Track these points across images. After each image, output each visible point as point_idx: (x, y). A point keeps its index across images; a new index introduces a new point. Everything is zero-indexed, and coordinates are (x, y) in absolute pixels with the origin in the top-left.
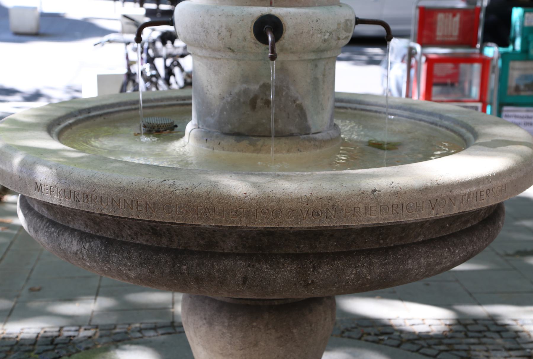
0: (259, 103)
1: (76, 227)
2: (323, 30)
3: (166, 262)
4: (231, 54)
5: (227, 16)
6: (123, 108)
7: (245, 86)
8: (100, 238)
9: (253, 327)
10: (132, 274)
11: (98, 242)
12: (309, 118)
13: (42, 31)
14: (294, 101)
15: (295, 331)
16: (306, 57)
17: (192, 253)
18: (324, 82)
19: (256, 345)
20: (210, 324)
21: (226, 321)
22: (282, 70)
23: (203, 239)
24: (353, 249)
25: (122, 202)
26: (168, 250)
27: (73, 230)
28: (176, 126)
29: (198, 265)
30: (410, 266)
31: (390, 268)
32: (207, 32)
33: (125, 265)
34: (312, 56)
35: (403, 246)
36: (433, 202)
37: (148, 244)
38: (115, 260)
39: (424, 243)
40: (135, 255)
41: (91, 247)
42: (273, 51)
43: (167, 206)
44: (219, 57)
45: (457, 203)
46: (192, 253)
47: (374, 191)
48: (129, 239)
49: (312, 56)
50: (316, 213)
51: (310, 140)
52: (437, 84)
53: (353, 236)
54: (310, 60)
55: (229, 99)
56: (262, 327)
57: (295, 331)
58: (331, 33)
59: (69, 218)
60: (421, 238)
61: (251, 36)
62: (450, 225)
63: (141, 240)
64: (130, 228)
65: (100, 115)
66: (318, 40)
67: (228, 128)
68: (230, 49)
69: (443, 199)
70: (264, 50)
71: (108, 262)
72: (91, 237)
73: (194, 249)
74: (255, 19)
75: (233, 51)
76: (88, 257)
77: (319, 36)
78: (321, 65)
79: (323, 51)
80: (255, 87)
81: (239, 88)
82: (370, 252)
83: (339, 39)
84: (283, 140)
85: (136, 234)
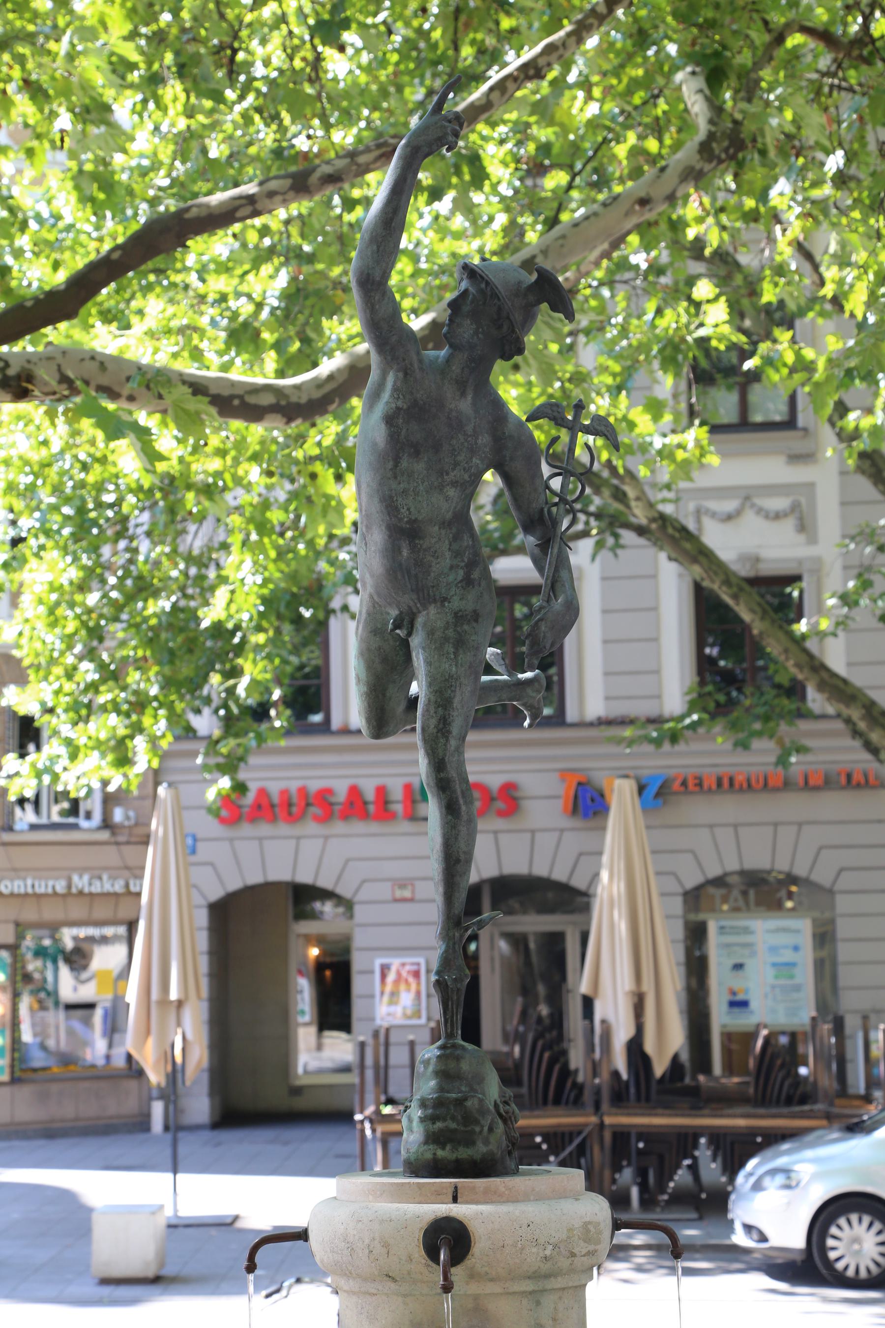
2: (541, 1241)
4: (393, 1285)
5: (382, 1222)
13: (167, 1271)
16: (517, 1287)
34: (529, 1286)
42: (446, 1278)
44: (373, 1291)
49: (529, 1286)
54: (523, 1292)
58: (555, 1246)
61: (419, 1253)
66: (532, 1258)
68: (388, 1276)
75: (394, 1280)
77: (534, 1250)
78: (548, 1302)
83: (573, 1255)
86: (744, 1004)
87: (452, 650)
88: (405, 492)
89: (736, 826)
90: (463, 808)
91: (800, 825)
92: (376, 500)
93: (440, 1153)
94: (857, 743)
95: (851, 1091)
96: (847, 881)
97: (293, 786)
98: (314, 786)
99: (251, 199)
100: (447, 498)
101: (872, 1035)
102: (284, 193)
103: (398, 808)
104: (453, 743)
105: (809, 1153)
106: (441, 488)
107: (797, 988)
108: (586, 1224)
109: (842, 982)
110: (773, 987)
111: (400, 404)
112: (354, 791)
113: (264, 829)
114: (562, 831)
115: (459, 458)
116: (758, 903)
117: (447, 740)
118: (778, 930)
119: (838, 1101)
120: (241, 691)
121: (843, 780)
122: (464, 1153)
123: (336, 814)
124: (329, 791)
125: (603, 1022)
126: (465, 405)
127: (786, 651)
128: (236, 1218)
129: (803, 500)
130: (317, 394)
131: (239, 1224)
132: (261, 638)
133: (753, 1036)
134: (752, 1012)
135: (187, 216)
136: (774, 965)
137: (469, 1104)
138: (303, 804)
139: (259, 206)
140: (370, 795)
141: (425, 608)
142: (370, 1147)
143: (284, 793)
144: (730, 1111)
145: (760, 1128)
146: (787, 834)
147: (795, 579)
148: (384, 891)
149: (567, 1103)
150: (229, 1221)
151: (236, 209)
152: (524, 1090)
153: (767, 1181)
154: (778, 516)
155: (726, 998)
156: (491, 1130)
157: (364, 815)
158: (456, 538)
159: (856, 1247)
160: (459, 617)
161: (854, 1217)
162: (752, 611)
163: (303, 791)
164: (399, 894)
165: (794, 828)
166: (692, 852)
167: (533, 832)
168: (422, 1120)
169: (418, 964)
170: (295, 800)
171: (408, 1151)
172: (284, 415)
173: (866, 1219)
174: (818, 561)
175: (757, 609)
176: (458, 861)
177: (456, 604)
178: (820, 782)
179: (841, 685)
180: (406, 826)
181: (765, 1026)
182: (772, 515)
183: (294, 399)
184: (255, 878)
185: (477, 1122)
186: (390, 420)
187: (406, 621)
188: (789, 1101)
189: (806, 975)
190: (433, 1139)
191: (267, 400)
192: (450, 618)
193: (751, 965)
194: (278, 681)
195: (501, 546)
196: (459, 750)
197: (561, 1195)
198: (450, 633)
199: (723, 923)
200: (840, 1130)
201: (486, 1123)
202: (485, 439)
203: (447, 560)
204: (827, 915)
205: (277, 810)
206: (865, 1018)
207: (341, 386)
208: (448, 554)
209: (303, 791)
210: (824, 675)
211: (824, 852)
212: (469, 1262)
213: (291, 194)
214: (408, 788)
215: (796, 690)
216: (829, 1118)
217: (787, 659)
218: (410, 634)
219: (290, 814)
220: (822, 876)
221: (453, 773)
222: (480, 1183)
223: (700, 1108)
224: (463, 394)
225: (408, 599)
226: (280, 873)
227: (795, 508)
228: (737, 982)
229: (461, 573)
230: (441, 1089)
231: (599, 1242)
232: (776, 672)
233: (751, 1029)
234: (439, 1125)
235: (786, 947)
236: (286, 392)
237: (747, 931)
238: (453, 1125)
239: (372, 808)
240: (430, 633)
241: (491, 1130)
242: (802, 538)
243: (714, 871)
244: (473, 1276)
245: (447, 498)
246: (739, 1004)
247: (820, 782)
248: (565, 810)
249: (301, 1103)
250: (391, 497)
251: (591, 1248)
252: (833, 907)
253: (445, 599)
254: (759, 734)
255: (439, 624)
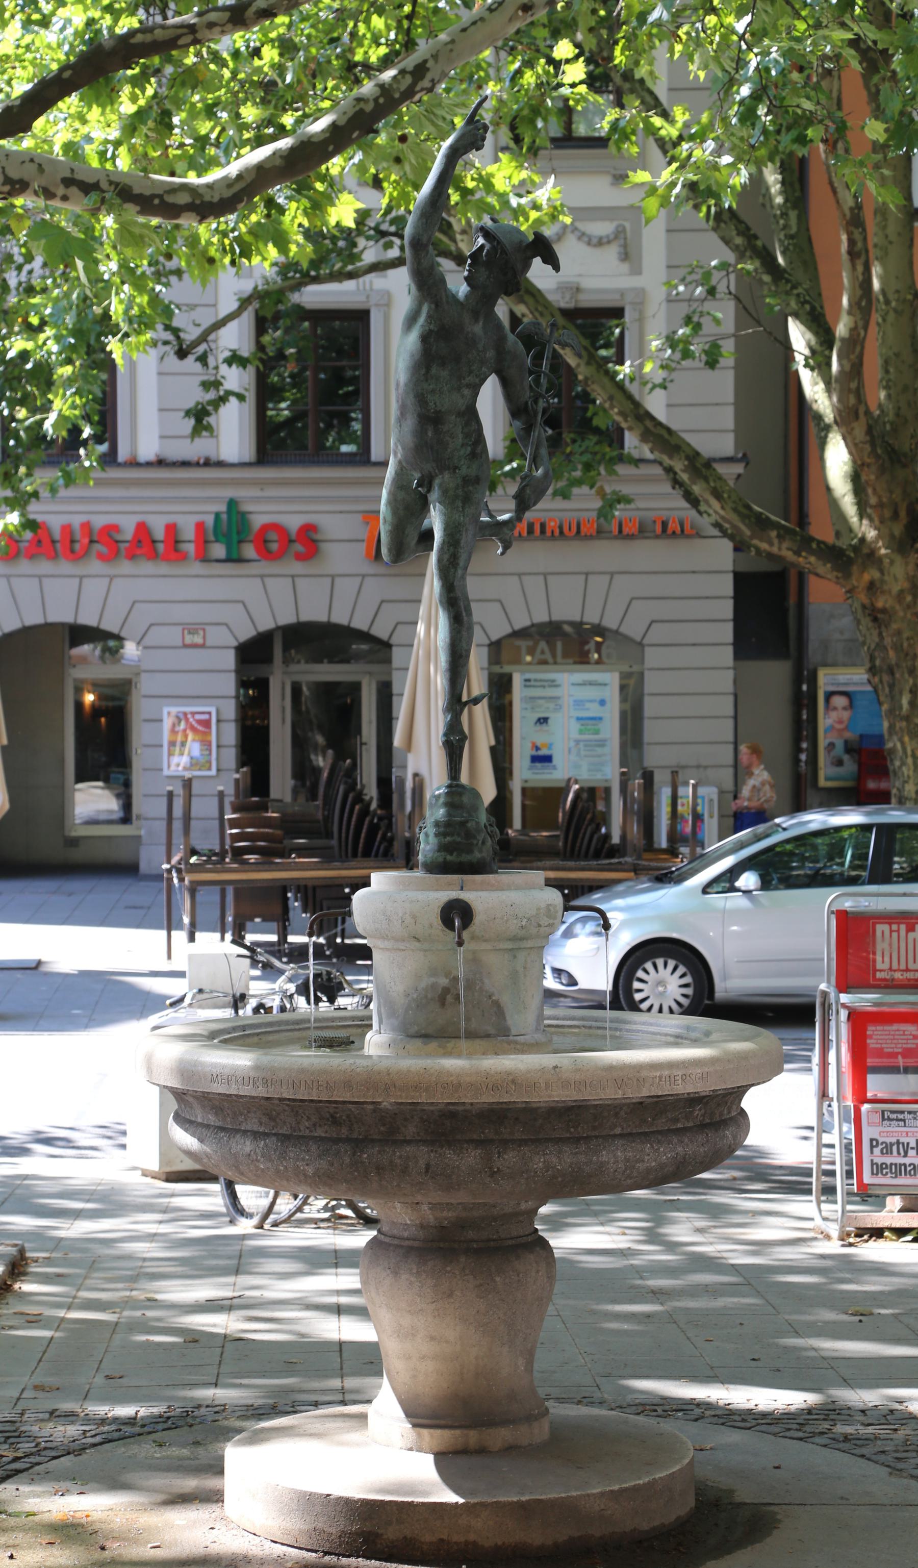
0: (449, 999)
1: (249, 1128)
3: (346, 1151)
4: (417, 944)
5: (412, 902)
6: (283, 1028)
7: (433, 980)
8: (275, 1134)
9: (447, 1272)
10: (310, 1171)
11: (274, 1138)
12: (508, 1018)
14: (490, 997)
15: (498, 1279)
17: (373, 1141)
18: (525, 976)
19: (450, 1295)
20: (396, 1273)
21: (414, 1267)
22: (474, 960)
23: (384, 1125)
24: (541, 1136)
25: (303, 1083)
26: (348, 1140)
27: (245, 1132)
28: (353, 1042)
29: (379, 1152)
30: (605, 1159)
31: (582, 1158)
32: (389, 920)
33: (303, 1159)
34: (509, 945)
35: (596, 1137)
36: (619, 1082)
37: (327, 1135)
38: (292, 1155)
39: (621, 1136)
40: (313, 1147)
41: (266, 1145)
42: (460, 937)
43: (348, 1084)
45: (647, 1085)
46: (373, 1141)
47: (556, 1067)
48: (307, 1133)
49: (509, 945)
50: (495, 1087)
51: (509, 1043)
52: (877, 1070)
53: (540, 1121)
55: (415, 996)
56: (457, 1272)
57: (498, 1279)
58: (529, 919)
59: (241, 1119)
60: (618, 1131)
61: (437, 922)
62: (653, 1120)
63: (320, 1132)
64: (309, 1119)
65: (258, 1034)
67: (414, 1029)
69: (629, 1079)
70: (452, 936)
71: (285, 1158)
72: (266, 1135)
73: (375, 1137)
74: (442, 904)
75: (418, 940)
76: (263, 1156)
78: (521, 956)
79: (522, 939)
80: (444, 982)
81: (426, 982)
82: (560, 1140)
83: (540, 926)
84: (478, 1042)
85: (314, 1125)
86: (548, 759)
87: (460, 504)
88: (433, 391)
89: (545, 575)
90: (465, 618)
91: (612, 574)
92: (411, 396)
93: (449, 858)
94: (678, 493)
95: (656, 846)
96: (657, 634)
97: (76, 521)
98: (99, 522)
99: (191, 29)
100: (463, 396)
101: (681, 791)
102: (224, 25)
103: (190, 548)
104: (460, 572)
105: (619, 902)
106: (459, 389)
107: (602, 743)
108: (549, 905)
109: (647, 737)
110: (577, 742)
111: (432, 327)
112: (142, 529)
113: (44, 566)
114: (364, 576)
115: (473, 368)
116: (565, 655)
117: (456, 570)
118: (584, 684)
119: (647, 855)
120: (48, 426)
121: (658, 528)
122: (465, 858)
123: (123, 552)
124: (115, 528)
125: (416, 775)
126: (478, 329)
127: (611, 398)
128: (39, 963)
129: (627, 225)
130: (228, 194)
131: (43, 969)
132: (67, 370)
133: (565, 790)
134: (555, 768)
135: (133, 41)
136: (578, 719)
137: (469, 825)
138: (86, 541)
139: (199, 36)
140: (159, 533)
141: (441, 473)
142: (177, 896)
143: (67, 529)
144: (539, 864)
145: (569, 880)
146: (598, 584)
147: (618, 313)
148: (173, 636)
149: (376, 856)
150: (33, 965)
151: (179, 37)
152: (334, 842)
153: (578, 928)
154: (600, 242)
155: (529, 752)
156: (483, 843)
157: (153, 555)
158: (467, 424)
159: (661, 989)
160: (466, 481)
161: (660, 962)
162: (580, 356)
163: (86, 526)
164: (189, 639)
165: (607, 578)
166: (500, 601)
167: (333, 577)
168: (436, 835)
169: (210, 713)
170: (78, 536)
171: (425, 856)
172: (198, 214)
173: (671, 963)
174: (641, 293)
175: (584, 353)
176: (461, 656)
177: (464, 471)
178: (634, 530)
179: (664, 433)
180: (197, 568)
181: (576, 782)
182: (595, 241)
183: (207, 198)
184: (34, 618)
185: (474, 837)
186: (425, 339)
187: (427, 482)
188: (597, 855)
189: (611, 729)
190: (443, 848)
191: (183, 199)
192: (459, 481)
193: (556, 720)
194: (87, 418)
195: (313, 273)
196: (463, 578)
197: (531, 887)
198: (460, 492)
199: (528, 676)
200: (650, 880)
201: (480, 838)
202: (491, 354)
203: (460, 439)
204: (636, 668)
205: (58, 546)
206: (674, 774)
207: (248, 185)
208: (460, 436)
209: (86, 526)
210: (649, 424)
211: (634, 602)
212: (472, 928)
213: (229, 26)
214: (200, 526)
215: (615, 437)
216: (637, 870)
217: (612, 407)
218: (429, 491)
219: (72, 551)
220: (633, 629)
221: (458, 593)
222: (478, 878)
223: (510, 861)
224: (476, 320)
225: (429, 467)
226: (61, 614)
227: (619, 234)
228: (541, 738)
229: (469, 449)
230: (449, 814)
231: (555, 918)
232: (595, 414)
233: (563, 785)
234: (448, 839)
235: (591, 701)
236: (200, 191)
237: (553, 684)
238: (459, 839)
239: (161, 547)
240: (445, 492)
241: (483, 843)
242: (625, 267)
243: (522, 621)
244: (473, 938)
245: (463, 396)
246: (542, 759)
247: (634, 530)
248: (368, 555)
249: (78, 855)
250: (422, 394)
251: (551, 921)
252: (642, 662)
253: (456, 468)
254: (578, 482)
255: (452, 485)
